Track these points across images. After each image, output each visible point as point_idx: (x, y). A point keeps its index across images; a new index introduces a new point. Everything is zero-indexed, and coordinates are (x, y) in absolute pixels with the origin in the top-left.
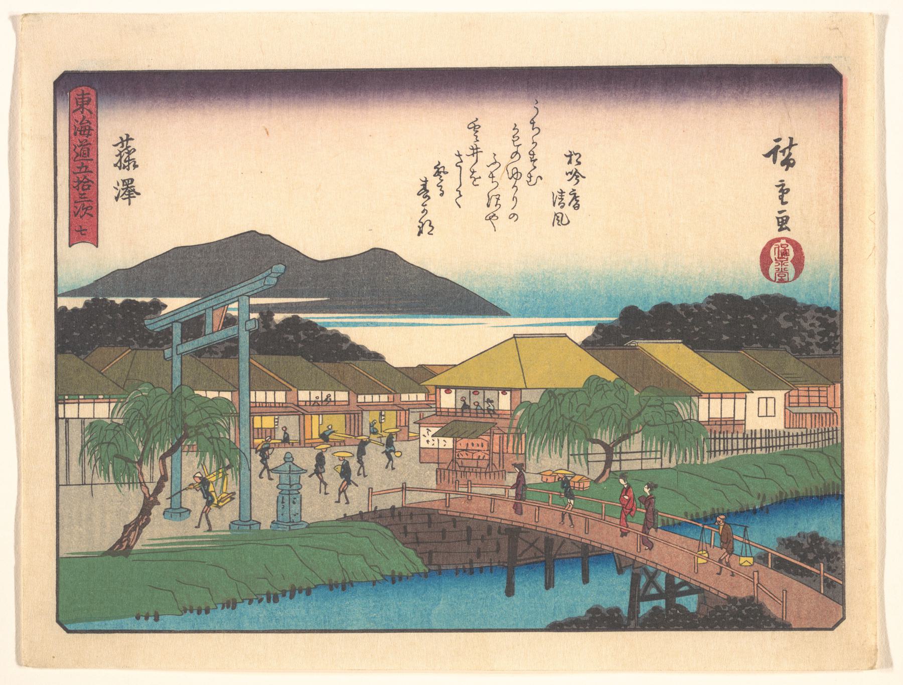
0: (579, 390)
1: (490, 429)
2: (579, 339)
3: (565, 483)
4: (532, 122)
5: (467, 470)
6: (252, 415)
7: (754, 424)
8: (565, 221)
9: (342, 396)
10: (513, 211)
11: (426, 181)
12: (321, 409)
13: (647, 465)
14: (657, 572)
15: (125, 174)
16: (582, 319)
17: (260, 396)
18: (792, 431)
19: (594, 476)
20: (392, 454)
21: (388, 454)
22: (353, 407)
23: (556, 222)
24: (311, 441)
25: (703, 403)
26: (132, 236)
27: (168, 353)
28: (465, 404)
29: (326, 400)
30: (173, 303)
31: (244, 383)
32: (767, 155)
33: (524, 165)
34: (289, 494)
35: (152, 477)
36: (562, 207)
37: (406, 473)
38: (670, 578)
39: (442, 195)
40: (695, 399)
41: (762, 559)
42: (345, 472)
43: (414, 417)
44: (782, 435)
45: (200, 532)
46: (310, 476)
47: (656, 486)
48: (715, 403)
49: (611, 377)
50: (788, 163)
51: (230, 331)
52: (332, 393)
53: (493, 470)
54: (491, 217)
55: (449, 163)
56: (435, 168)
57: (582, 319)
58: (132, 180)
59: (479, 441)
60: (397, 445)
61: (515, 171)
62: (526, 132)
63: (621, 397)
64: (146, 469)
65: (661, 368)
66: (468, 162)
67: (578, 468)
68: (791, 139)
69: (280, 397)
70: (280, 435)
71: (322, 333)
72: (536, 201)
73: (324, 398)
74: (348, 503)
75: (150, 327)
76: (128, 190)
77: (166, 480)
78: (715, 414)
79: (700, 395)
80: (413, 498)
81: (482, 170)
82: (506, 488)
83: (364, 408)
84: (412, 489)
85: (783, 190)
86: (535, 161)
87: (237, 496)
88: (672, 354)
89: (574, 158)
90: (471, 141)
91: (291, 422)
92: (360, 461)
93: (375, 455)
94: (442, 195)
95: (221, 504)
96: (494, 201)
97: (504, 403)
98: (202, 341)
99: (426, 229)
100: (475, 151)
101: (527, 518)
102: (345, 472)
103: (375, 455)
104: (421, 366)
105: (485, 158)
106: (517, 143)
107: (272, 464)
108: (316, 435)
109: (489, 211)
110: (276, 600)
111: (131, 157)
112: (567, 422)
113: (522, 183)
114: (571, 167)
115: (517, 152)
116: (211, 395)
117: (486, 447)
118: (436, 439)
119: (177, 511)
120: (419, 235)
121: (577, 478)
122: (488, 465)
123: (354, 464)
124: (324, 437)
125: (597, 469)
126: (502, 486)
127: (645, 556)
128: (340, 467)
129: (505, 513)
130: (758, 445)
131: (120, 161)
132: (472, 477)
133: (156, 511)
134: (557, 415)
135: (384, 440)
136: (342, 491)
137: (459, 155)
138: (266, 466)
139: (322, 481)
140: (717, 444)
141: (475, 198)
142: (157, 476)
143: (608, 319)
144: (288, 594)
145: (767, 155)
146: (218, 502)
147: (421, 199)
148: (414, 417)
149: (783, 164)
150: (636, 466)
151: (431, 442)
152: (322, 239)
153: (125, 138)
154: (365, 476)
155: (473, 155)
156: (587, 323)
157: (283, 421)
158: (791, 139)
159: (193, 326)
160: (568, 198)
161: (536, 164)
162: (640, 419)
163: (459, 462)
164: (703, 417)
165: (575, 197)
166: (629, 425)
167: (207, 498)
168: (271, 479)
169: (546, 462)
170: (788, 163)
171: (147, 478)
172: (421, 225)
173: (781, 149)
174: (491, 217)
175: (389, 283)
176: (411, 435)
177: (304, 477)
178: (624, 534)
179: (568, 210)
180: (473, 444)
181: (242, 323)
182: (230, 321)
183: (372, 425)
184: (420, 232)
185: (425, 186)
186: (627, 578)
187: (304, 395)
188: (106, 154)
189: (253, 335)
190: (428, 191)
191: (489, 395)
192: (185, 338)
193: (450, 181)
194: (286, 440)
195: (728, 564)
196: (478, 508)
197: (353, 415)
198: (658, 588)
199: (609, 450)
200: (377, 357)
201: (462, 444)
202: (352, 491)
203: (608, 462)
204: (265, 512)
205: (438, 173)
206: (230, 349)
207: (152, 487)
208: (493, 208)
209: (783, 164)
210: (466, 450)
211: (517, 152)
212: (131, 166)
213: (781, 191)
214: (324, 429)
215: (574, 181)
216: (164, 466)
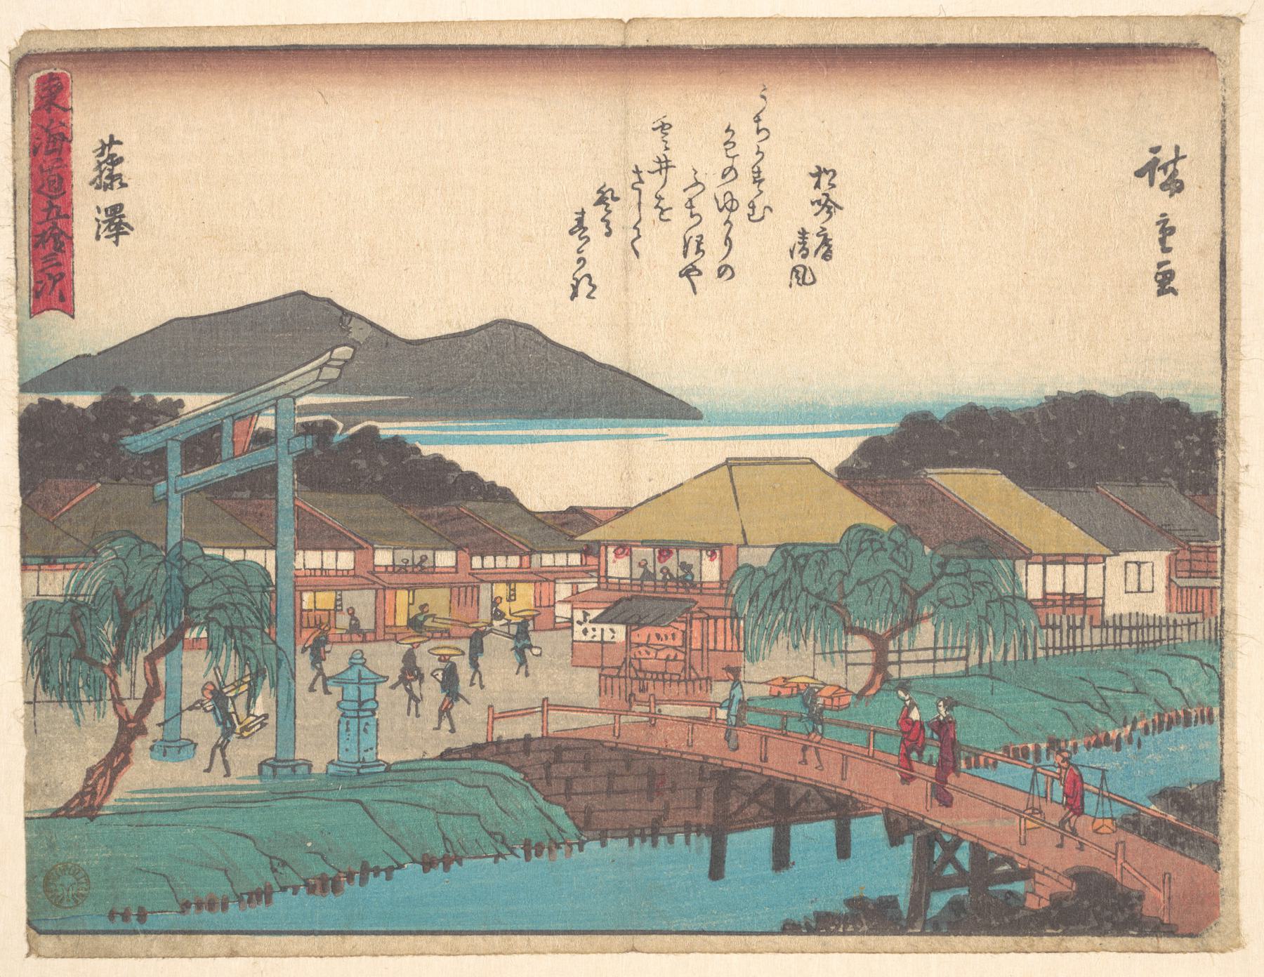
0: (833, 547)
1: (687, 613)
2: (830, 464)
3: (808, 695)
4: (757, 119)
5: (649, 675)
6: (298, 590)
7: (1118, 605)
8: (809, 279)
9: (446, 559)
10: (724, 262)
11: (583, 212)
12: (412, 578)
13: (943, 668)
14: (958, 842)
15: (108, 199)
16: (837, 427)
17: (312, 559)
18: (1181, 618)
19: (856, 688)
20: (527, 651)
21: (520, 652)
22: (462, 576)
23: (795, 280)
24: (394, 630)
25: (1035, 570)
26: (120, 296)
27: (161, 487)
28: (646, 572)
29: (419, 564)
30: (194, 402)
31: (287, 538)
32: (1139, 174)
33: (744, 190)
34: (359, 713)
35: (132, 692)
36: (804, 256)
37: (551, 685)
38: (978, 851)
39: (608, 234)
40: (1020, 564)
41: (1132, 823)
42: (450, 680)
43: (564, 590)
44: (1164, 622)
45: (206, 780)
46: (393, 687)
47: (957, 704)
48: (1054, 571)
49: (882, 522)
50: (1175, 186)
51: (264, 455)
52: (429, 553)
53: (691, 678)
54: (687, 273)
55: (620, 184)
56: (599, 191)
57: (837, 427)
58: (121, 206)
59: (669, 631)
60: (535, 638)
61: (728, 196)
62: (745, 130)
63: (902, 560)
64: (123, 681)
65: (964, 511)
66: (652, 184)
67: (830, 673)
68: (1177, 148)
69: (346, 560)
70: (343, 621)
71: (413, 457)
72: (763, 249)
73: (417, 561)
74: (453, 731)
75: (132, 448)
76: (116, 223)
77: (159, 694)
78: (1054, 586)
79: (1028, 557)
80: (559, 723)
81: (675, 196)
82: (714, 706)
83: (481, 578)
84: (557, 707)
85: (1166, 230)
86: (760, 182)
87: (272, 720)
88: (986, 492)
89: (825, 179)
90: (660, 151)
91: (362, 602)
92: (474, 665)
93: (498, 647)
94: (608, 234)
95: (246, 734)
96: (693, 246)
97: (710, 571)
98: (212, 472)
99: (584, 288)
100: (664, 165)
101: (747, 755)
102: (450, 680)
103: (498, 647)
104: (573, 510)
105: (679, 177)
106: (731, 153)
107: (329, 668)
108: (402, 620)
109: (685, 263)
110: (336, 889)
111: (117, 170)
112: (812, 601)
113: (739, 217)
114: (817, 195)
115: (732, 168)
116: (233, 555)
117: (679, 642)
118: (598, 627)
119: (174, 746)
120: (572, 299)
121: (827, 692)
122: (684, 669)
123: (463, 666)
124: (414, 623)
125: (860, 677)
126: (703, 703)
127: (938, 818)
128: (440, 673)
129: (709, 744)
130: (1125, 639)
131: (100, 176)
132: (655, 689)
133: (140, 745)
134: (798, 585)
135: (514, 630)
136: (444, 712)
137: (637, 172)
138: (321, 672)
139: (412, 697)
140: (1058, 639)
141: (662, 245)
142: (140, 691)
143: (884, 426)
144: (357, 876)
145: (1139, 174)
146: (242, 730)
147: (575, 241)
148: (564, 590)
149: (1163, 186)
150: (927, 669)
151: (591, 633)
152: (420, 303)
153: (107, 141)
154: (482, 687)
155: (660, 170)
156: (852, 434)
157: (350, 598)
158: (1177, 148)
159: (202, 446)
160: (814, 242)
161: (762, 187)
162: (931, 594)
163: (636, 663)
164: (1035, 593)
165: (826, 242)
166: (914, 605)
167: (224, 724)
168: (327, 692)
169: (781, 663)
170: (1175, 186)
171: (125, 693)
172: (574, 283)
173: (1161, 164)
174: (687, 273)
175: (525, 375)
176: (558, 620)
177: (382, 689)
178: (907, 779)
179: (814, 262)
180: (658, 636)
181: (282, 441)
182: (263, 438)
183: (495, 602)
184: (574, 295)
185: (580, 221)
186: (907, 850)
187: (383, 558)
188: (83, 162)
189: (302, 461)
190: (585, 229)
191: (689, 556)
192: (190, 461)
193: (621, 214)
194: (355, 628)
195: (1074, 832)
196: (670, 738)
197: (465, 587)
198: (958, 866)
199: (880, 645)
200: (506, 496)
201: (641, 635)
202: (459, 710)
203: (880, 666)
204: (318, 744)
205: (601, 201)
206: (260, 482)
207: (132, 707)
208: (692, 257)
209: (1163, 186)
210: (647, 645)
211: (732, 168)
212: (116, 184)
213: (1163, 230)
214: (415, 611)
215: (824, 215)
216: (154, 672)
